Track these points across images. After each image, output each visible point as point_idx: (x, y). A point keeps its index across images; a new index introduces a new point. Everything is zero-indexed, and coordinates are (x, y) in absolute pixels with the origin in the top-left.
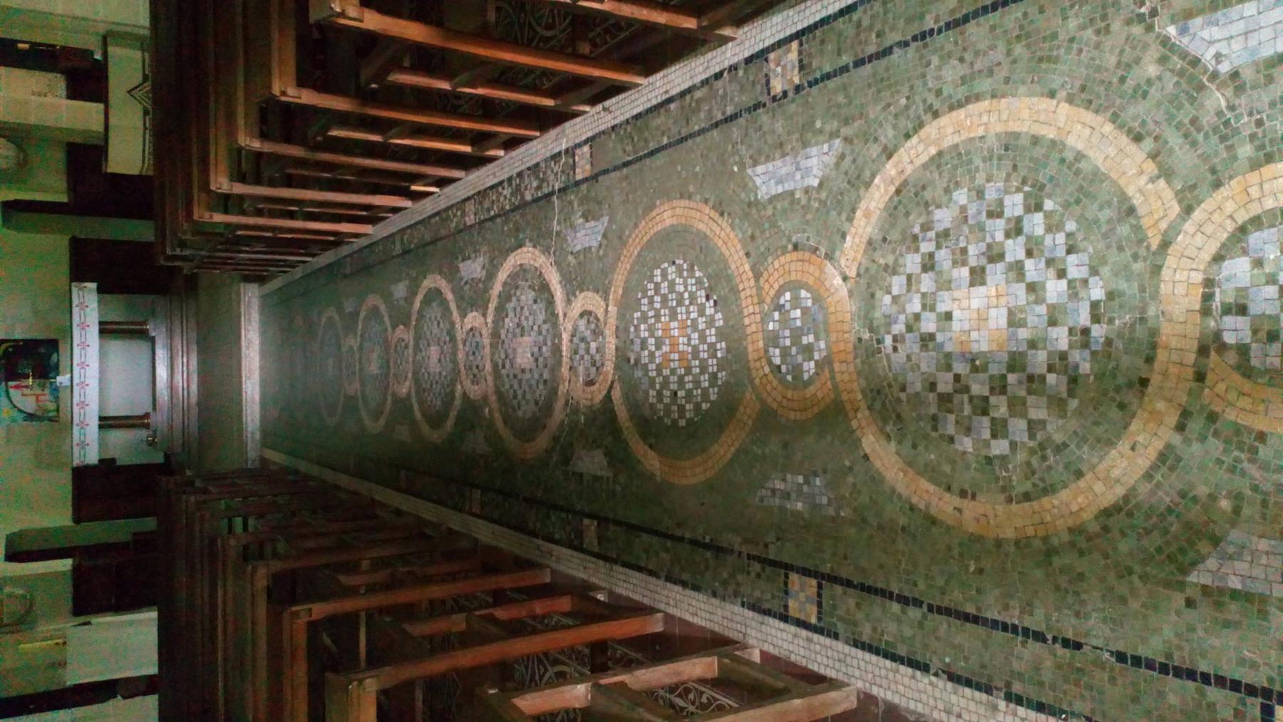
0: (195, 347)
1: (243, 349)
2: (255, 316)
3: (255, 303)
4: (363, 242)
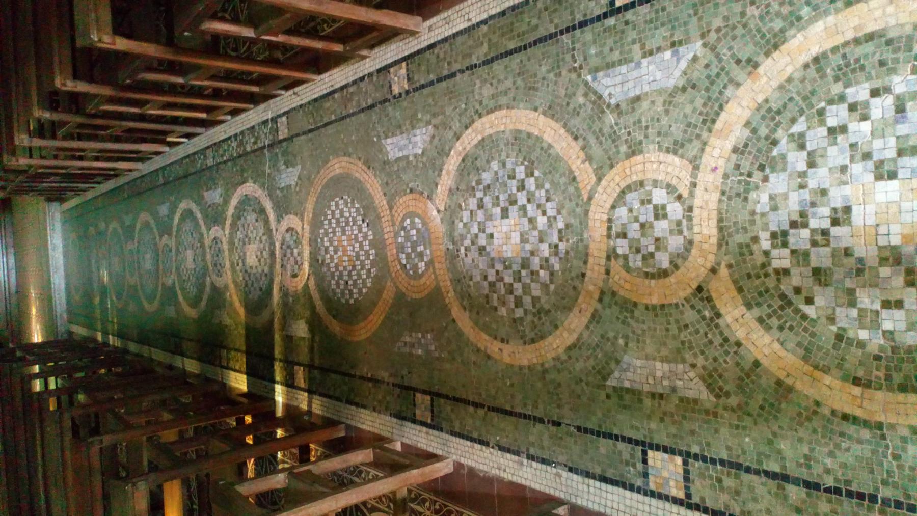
0: (12, 250)
1: (50, 251)
2: (58, 226)
3: (58, 216)
4: (135, 175)
